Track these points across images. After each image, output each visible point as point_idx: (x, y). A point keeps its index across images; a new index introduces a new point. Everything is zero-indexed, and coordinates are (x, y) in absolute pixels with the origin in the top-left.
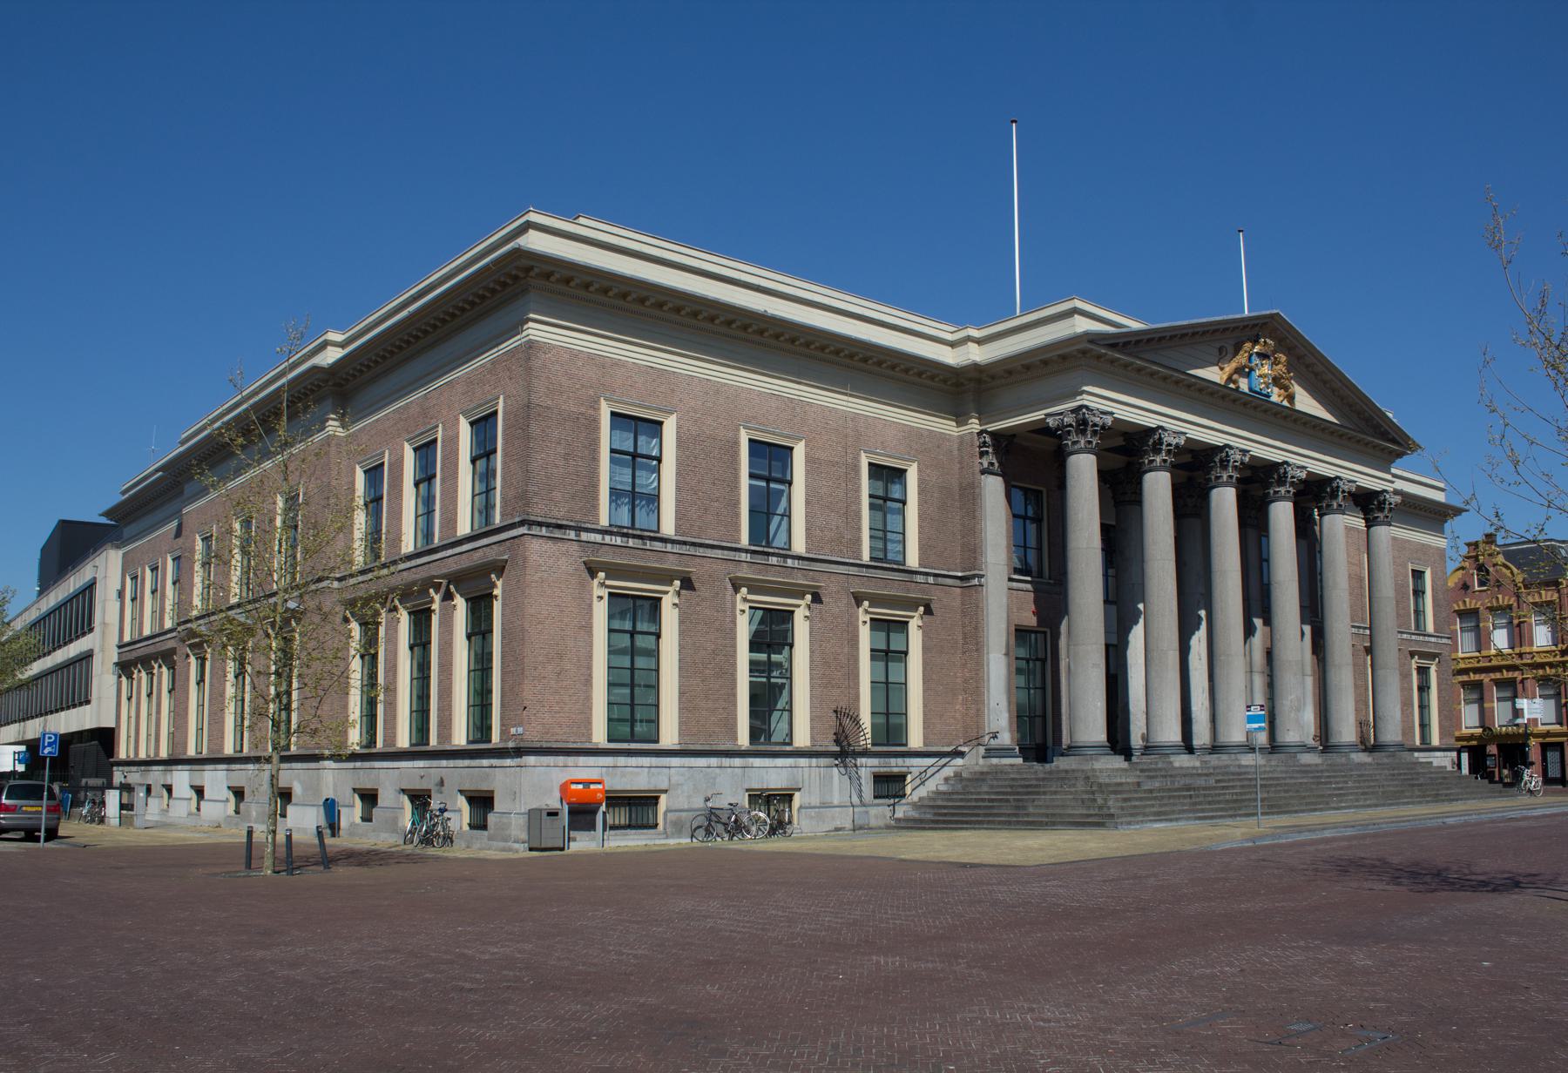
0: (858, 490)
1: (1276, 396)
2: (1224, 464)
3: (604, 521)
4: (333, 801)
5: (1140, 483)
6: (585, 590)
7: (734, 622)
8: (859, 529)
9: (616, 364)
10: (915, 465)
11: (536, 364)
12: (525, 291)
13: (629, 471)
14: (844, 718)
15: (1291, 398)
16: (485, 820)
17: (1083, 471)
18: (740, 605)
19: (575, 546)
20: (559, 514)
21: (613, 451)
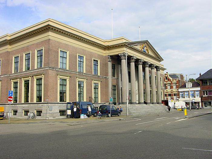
0: (92, 63)
1: (147, 52)
2: (141, 61)
3: (59, 68)
4: (60, 111)
5: (121, 61)
6: (56, 77)
7: (76, 83)
8: (92, 69)
9: (61, 43)
10: (85, 56)
11: (50, 42)
12: (49, 31)
13: (39, 55)
14: (90, 98)
15: (148, 52)
16: (16, 113)
17: (124, 62)
18: (93, 83)
19: (55, 71)
20: (53, 66)
21: (60, 56)
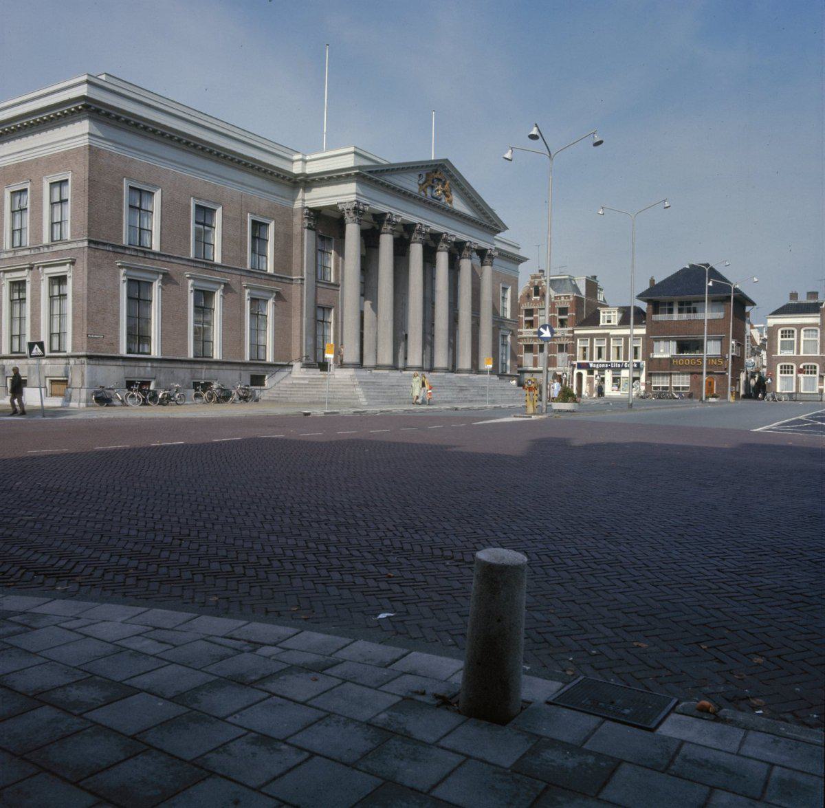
15: (451, 202)
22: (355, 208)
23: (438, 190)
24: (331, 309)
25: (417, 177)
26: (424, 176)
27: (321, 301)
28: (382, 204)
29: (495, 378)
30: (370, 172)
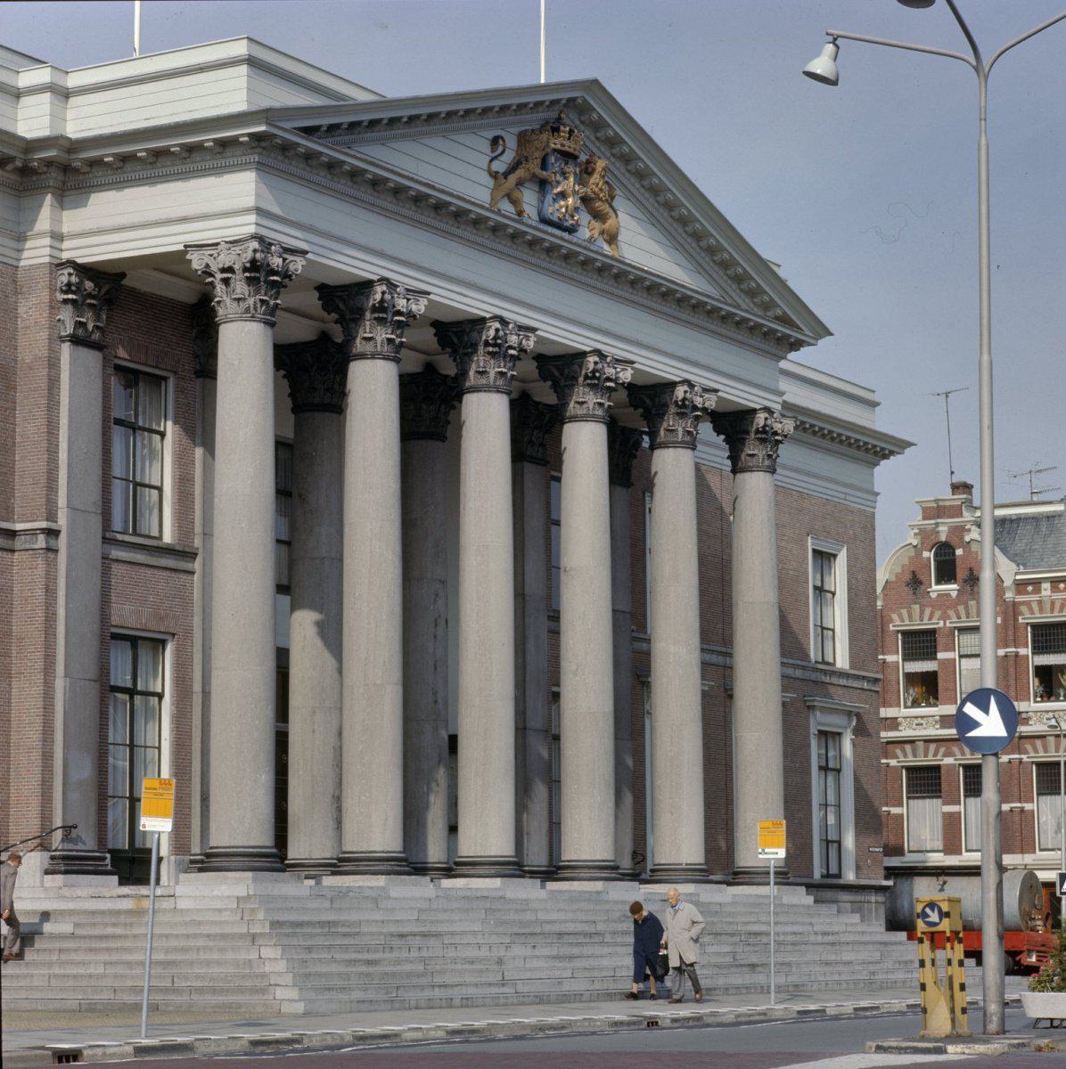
15: (612, 239)
22: (254, 266)
23: (563, 195)
24: (163, 642)
25: (485, 146)
26: (511, 142)
27: (126, 615)
28: (357, 245)
29: (800, 897)
30: (309, 131)
